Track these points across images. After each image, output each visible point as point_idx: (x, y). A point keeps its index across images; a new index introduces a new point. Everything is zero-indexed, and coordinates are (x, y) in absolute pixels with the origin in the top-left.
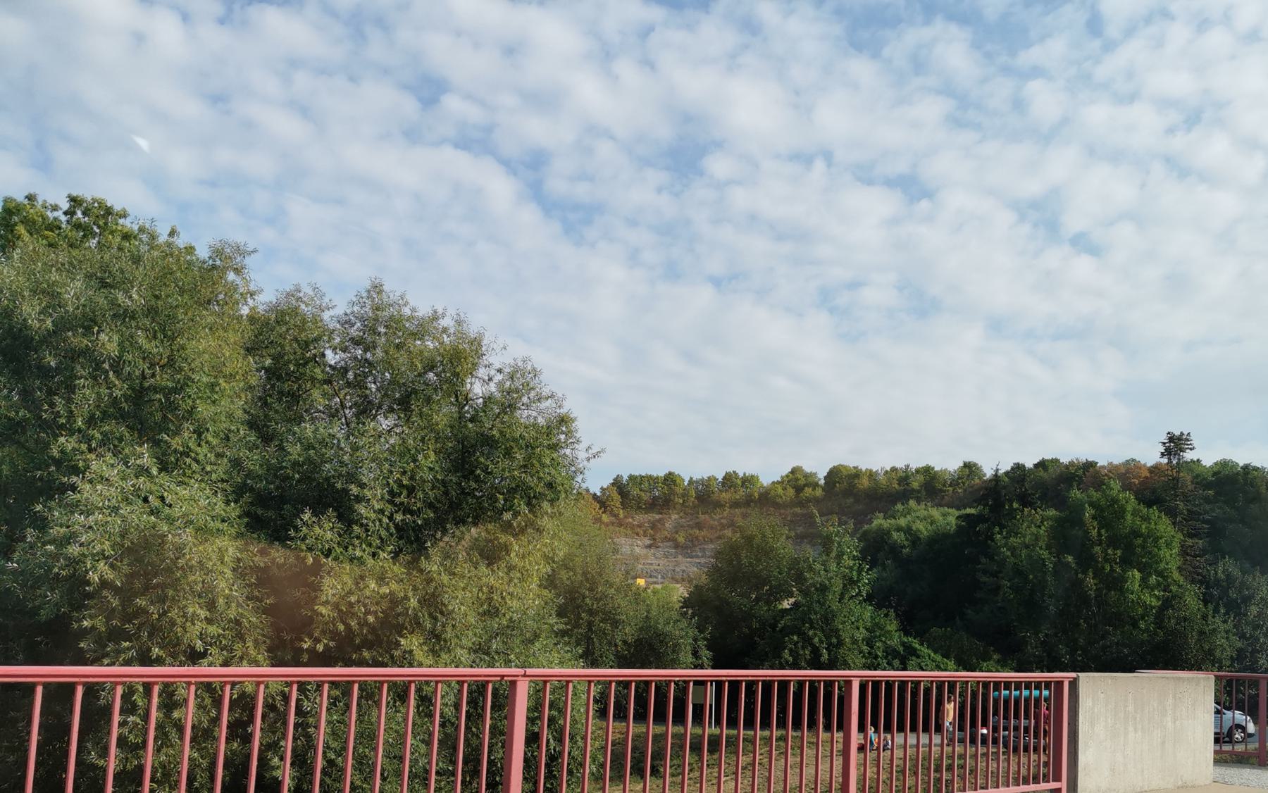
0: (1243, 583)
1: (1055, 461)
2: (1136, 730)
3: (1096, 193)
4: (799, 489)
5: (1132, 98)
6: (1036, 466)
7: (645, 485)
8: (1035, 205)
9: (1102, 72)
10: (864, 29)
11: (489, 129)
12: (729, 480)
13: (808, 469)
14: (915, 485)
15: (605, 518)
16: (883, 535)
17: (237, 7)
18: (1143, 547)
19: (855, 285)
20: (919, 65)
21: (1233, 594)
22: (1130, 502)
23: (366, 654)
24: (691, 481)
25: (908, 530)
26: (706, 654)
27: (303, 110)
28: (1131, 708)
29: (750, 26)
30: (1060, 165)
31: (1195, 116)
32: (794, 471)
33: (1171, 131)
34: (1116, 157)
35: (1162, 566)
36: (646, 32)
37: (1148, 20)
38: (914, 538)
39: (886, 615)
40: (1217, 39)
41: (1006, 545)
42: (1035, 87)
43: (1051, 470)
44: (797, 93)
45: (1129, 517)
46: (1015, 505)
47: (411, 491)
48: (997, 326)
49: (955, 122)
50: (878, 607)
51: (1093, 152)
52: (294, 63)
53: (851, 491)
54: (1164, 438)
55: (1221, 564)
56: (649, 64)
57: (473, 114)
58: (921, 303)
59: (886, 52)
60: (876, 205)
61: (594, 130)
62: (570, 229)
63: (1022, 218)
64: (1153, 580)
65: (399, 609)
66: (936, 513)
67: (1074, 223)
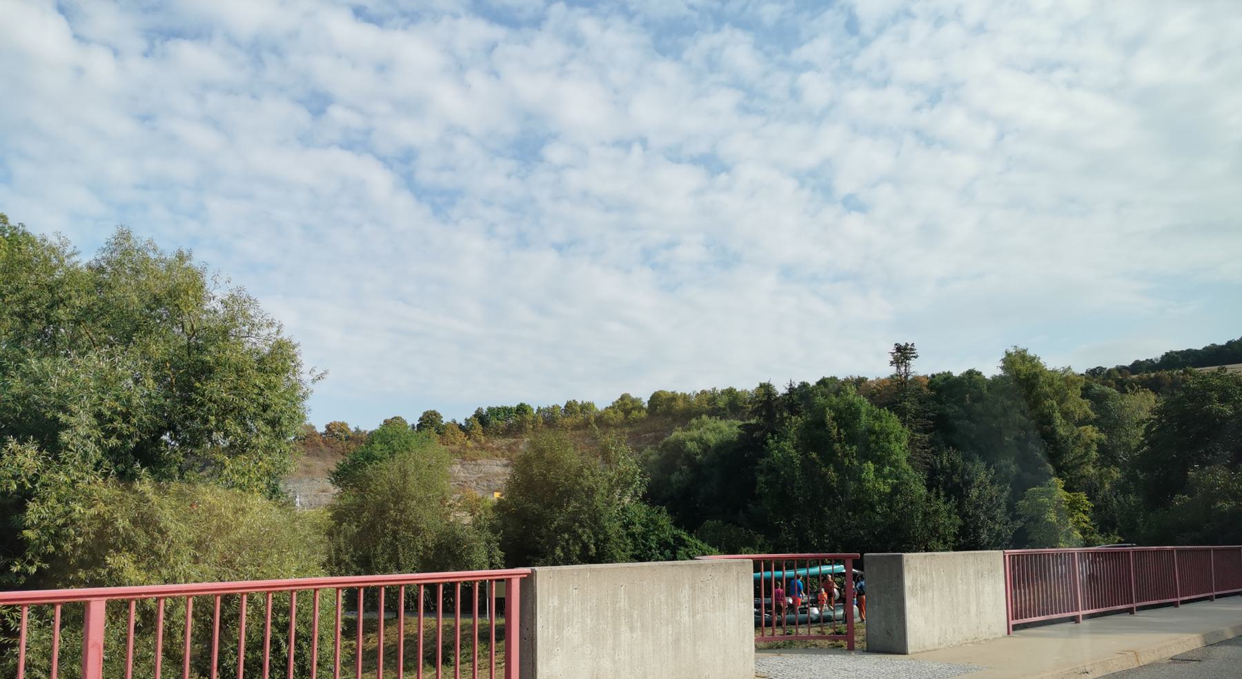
0: (964, 470)
1: (834, 379)
2: (632, 629)
3: (862, 161)
4: (627, 412)
5: (885, 83)
6: (818, 383)
7: (502, 415)
8: (812, 173)
9: (860, 63)
10: (668, 36)
11: (368, 132)
12: (570, 407)
13: (634, 395)
14: (721, 404)
15: (470, 444)
16: (680, 444)
17: (157, 43)
18: (877, 443)
19: (670, 245)
20: (712, 64)
21: (956, 479)
22: (865, 405)
23: (81, 574)
24: (539, 410)
25: (700, 440)
26: (499, 554)
27: (214, 123)
28: (623, 603)
29: (575, 40)
30: (831, 140)
31: (937, 95)
32: (622, 398)
33: (918, 108)
34: (874, 131)
35: (894, 457)
36: (491, 48)
37: (895, 19)
38: (705, 447)
39: (659, 512)
40: (951, 32)
41: (777, 448)
42: (806, 78)
43: (830, 386)
44: (616, 92)
45: (864, 417)
46: (785, 415)
47: (126, 417)
48: (787, 272)
49: (744, 110)
50: (652, 504)
51: (855, 128)
52: (206, 86)
53: (669, 412)
54: (892, 349)
55: (945, 455)
56: (494, 74)
57: (355, 121)
58: (725, 257)
59: (686, 55)
60: (685, 178)
61: (453, 130)
62: (437, 210)
63: (802, 185)
64: (887, 469)
65: (110, 530)
66: (723, 424)
67: (844, 186)
